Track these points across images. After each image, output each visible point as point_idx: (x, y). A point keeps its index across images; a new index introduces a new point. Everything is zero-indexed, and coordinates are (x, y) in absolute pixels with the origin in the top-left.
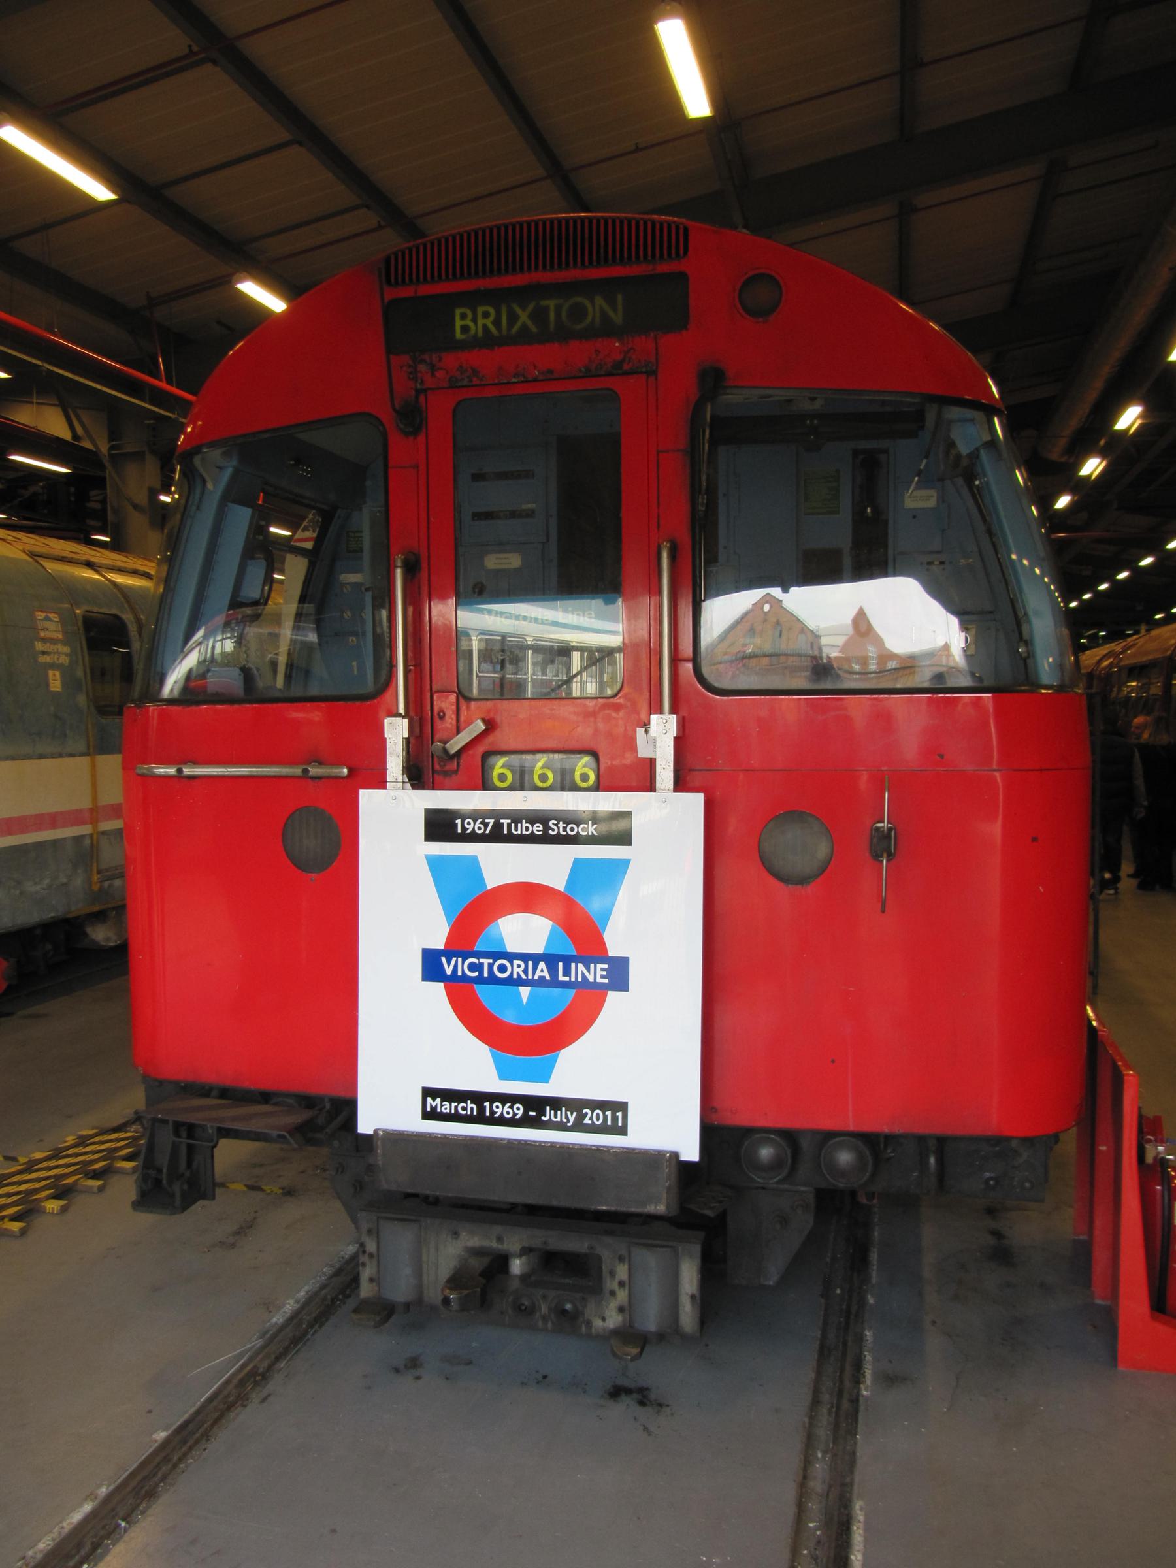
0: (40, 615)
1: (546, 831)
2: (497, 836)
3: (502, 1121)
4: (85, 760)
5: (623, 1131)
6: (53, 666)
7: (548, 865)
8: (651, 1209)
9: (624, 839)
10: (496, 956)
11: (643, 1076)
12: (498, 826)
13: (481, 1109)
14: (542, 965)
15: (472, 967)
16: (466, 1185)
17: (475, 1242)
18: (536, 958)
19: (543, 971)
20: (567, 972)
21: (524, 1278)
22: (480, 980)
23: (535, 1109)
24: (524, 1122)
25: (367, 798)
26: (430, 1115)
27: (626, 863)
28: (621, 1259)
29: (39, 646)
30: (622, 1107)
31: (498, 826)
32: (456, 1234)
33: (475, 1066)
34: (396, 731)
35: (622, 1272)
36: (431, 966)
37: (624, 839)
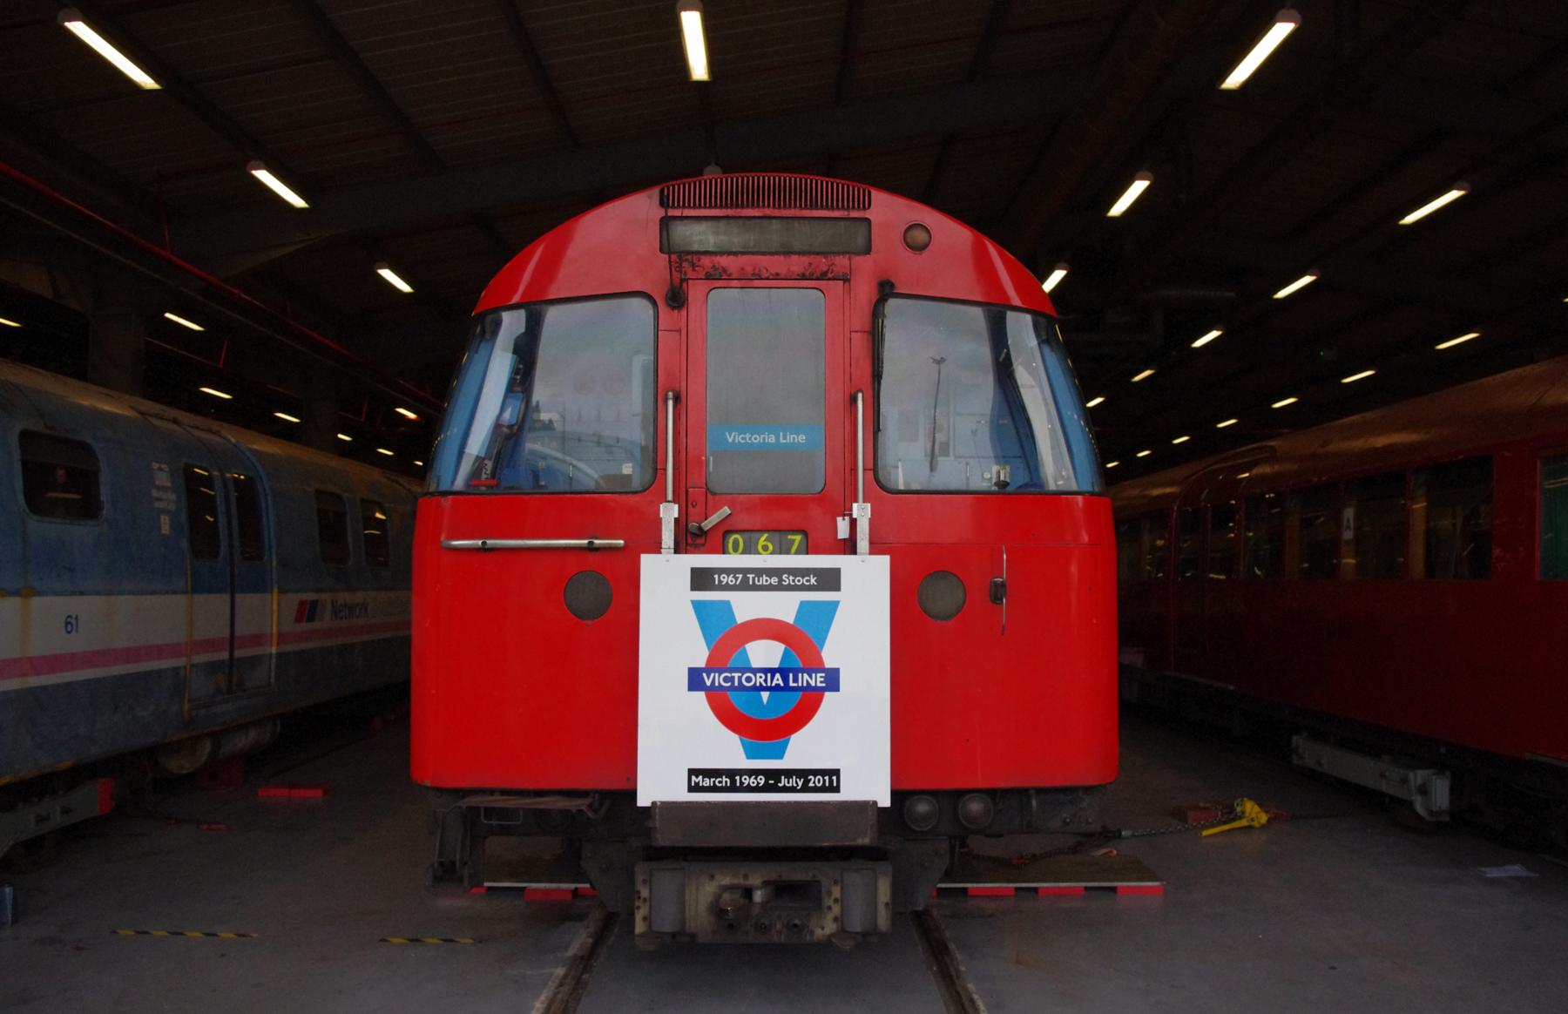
0: (155, 465)
1: (779, 581)
2: (745, 586)
3: (750, 789)
4: (181, 599)
5: (837, 790)
6: (163, 511)
7: (783, 606)
8: (860, 842)
9: (837, 588)
10: (743, 670)
11: (853, 748)
12: (745, 579)
13: (733, 781)
14: (778, 676)
15: (726, 679)
16: (723, 838)
17: (727, 881)
18: (773, 671)
19: (778, 679)
20: (795, 680)
21: (763, 904)
22: (732, 688)
23: (773, 780)
24: (766, 788)
25: (646, 559)
26: (693, 788)
27: (836, 604)
28: (836, 882)
29: (155, 493)
30: (836, 772)
31: (745, 579)
32: (712, 877)
33: (729, 751)
34: (669, 513)
35: (836, 892)
36: (695, 680)
37: (837, 588)
